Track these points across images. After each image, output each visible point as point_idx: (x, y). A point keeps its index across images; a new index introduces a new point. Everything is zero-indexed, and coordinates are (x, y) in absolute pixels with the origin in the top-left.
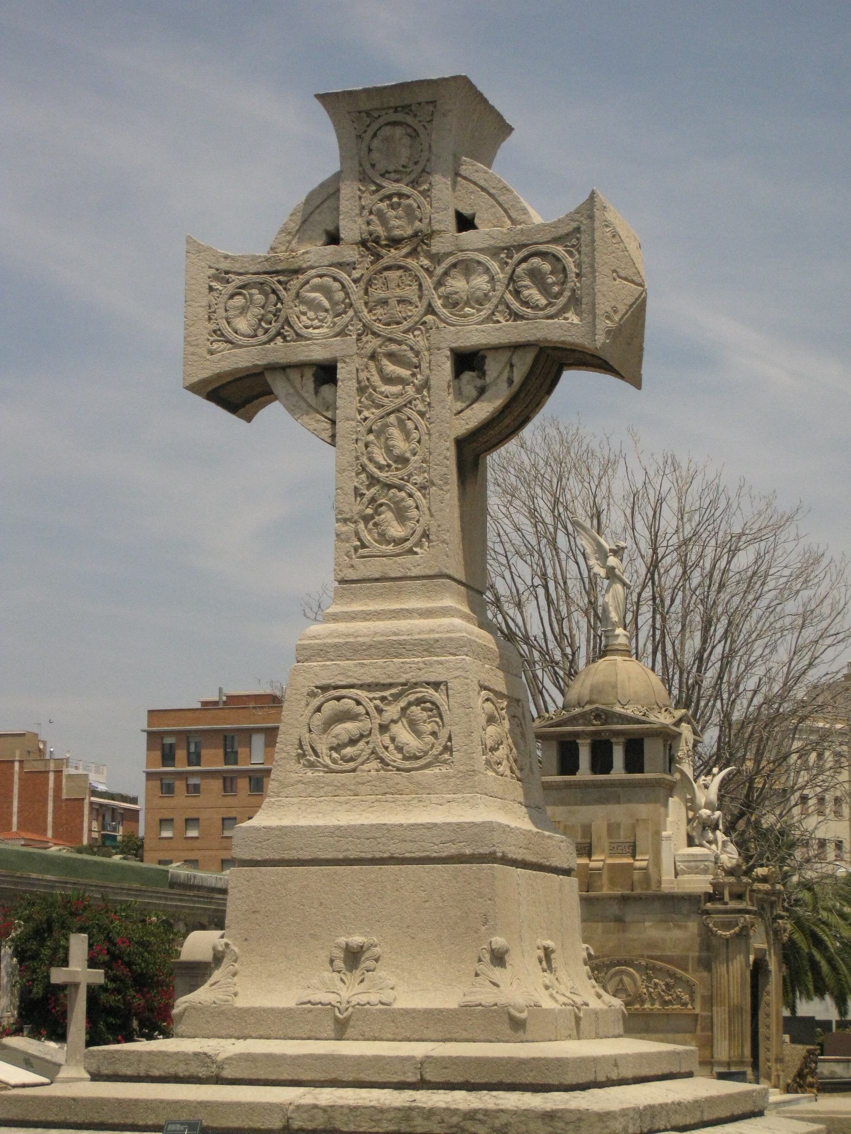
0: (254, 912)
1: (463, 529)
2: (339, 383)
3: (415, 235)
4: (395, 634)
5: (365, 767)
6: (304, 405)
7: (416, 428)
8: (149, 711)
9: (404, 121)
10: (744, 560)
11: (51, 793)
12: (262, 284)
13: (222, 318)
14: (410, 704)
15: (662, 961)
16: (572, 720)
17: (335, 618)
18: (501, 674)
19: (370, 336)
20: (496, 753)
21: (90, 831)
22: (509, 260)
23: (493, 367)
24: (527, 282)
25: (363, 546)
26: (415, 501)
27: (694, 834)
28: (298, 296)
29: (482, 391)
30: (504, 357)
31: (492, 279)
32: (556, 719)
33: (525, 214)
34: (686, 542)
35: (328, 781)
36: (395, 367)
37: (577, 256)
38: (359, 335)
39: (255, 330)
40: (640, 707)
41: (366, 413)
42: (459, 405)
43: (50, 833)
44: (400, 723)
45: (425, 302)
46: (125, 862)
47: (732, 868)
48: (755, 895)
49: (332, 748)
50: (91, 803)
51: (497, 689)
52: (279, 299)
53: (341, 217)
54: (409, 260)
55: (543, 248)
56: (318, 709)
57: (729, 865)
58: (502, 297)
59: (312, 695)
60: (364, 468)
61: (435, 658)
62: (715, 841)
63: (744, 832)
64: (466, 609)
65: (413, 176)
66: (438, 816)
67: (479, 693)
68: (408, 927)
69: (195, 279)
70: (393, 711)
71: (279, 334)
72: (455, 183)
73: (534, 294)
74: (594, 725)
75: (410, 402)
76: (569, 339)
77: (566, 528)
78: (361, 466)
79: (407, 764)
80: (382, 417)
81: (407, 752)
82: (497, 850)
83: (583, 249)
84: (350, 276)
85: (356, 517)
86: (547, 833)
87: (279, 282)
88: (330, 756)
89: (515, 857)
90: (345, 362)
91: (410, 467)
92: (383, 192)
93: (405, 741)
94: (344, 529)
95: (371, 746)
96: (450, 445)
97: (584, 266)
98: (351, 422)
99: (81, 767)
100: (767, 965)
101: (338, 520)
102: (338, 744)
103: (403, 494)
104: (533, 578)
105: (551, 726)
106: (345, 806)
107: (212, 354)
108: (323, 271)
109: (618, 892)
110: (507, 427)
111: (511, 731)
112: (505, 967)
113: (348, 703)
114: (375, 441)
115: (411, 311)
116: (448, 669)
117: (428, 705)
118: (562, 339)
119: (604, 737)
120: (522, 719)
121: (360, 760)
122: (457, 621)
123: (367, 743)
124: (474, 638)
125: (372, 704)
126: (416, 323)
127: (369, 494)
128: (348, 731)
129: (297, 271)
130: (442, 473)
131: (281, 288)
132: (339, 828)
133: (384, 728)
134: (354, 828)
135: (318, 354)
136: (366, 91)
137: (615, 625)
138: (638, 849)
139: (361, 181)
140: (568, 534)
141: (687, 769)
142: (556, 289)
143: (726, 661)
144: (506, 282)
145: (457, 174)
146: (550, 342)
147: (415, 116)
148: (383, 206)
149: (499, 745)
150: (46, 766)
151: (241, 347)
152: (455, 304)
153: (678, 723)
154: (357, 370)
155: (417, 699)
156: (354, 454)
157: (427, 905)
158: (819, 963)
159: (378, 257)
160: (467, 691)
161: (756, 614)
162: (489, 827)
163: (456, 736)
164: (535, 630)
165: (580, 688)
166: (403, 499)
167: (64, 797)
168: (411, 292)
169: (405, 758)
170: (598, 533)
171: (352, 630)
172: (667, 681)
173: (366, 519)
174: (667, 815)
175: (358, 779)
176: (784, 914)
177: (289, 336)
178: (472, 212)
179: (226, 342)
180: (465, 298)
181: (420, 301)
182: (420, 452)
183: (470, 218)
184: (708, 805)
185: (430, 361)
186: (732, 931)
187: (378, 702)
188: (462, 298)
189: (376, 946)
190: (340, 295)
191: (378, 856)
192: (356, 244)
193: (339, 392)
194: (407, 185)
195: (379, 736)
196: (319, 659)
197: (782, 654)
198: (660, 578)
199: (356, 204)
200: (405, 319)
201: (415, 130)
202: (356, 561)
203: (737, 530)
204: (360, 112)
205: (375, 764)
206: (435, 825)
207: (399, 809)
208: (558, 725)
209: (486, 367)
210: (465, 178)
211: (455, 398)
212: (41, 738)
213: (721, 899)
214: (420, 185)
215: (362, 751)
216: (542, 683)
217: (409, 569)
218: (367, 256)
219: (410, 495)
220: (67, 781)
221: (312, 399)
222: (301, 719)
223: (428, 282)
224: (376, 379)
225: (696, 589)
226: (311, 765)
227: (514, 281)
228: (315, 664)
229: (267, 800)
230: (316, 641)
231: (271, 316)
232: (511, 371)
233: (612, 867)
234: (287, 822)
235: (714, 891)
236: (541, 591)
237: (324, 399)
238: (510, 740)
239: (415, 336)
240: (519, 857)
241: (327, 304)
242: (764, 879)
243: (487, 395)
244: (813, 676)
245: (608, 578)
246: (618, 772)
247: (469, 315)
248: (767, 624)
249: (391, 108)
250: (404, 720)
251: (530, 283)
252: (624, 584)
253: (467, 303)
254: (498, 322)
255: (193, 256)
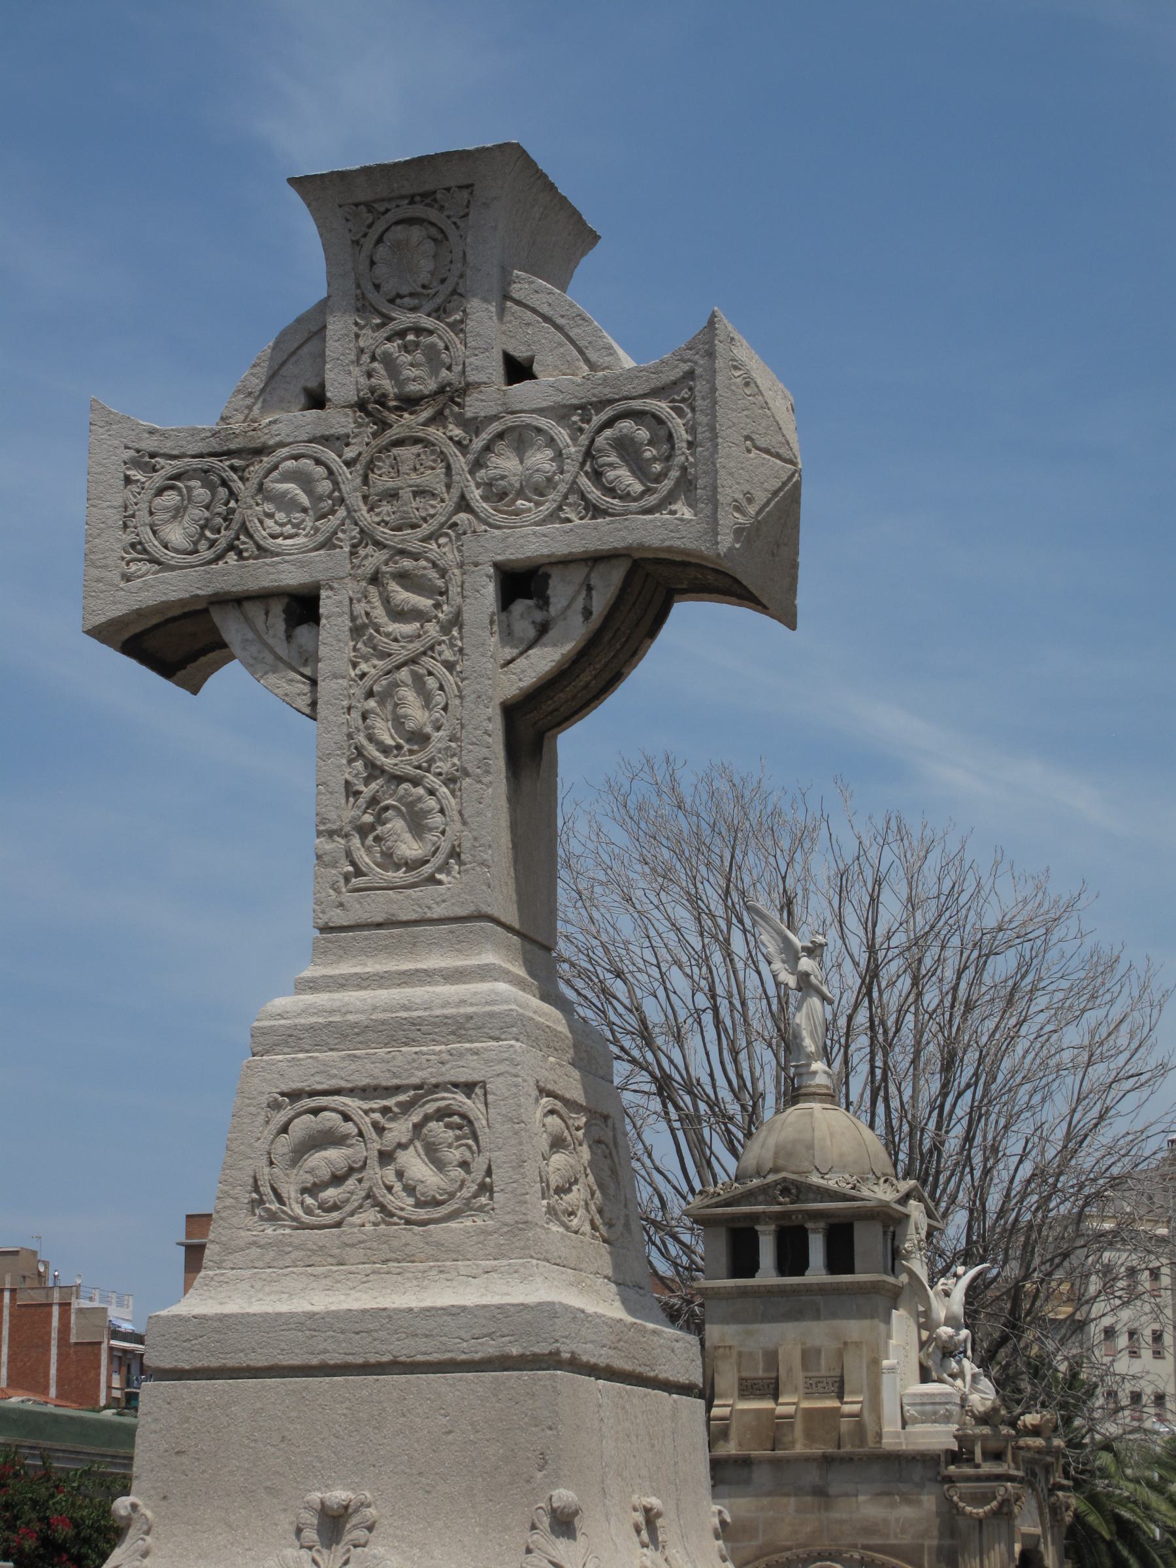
0: (178, 1453)
1: (515, 846)
2: (323, 621)
3: (441, 390)
4: (406, 1008)
5: (356, 1219)
6: (270, 658)
7: (441, 688)
8: (188, 1217)
9: (422, 215)
10: (1001, 967)
11: (54, 1335)
12: (206, 472)
13: (144, 525)
14: (427, 1118)
15: (885, 1553)
16: (748, 1197)
17: (313, 985)
18: (576, 1074)
19: (370, 548)
20: (567, 1198)
21: (109, 1387)
22: (585, 426)
23: (560, 592)
24: (613, 458)
25: (359, 873)
26: (439, 801)
27: (930, 1363)
28: (260, 488)
29: (543, 629)
30: (578, 574)
31: (559, 456)
32: (724, 1195)
33: (611, 354)
34: (917, 942)
35: (297, 1242)
36: (410, 594)
37: (690, 415)
38: (354, 546)
39: (196, 543)
40: (847, 1176)
41: (364, 667)
42: (509, 653)
43: (53, 1391)
44: (411, 1148)
45: (455, 492)
46: (118, 1419)
47: (986, 1413)
48: (1022, 1453)
49: (304, 1191)
50: (111, 1349)
51: (568, 1096)
52: (232, 494)
53: (328, 366)
54: (431, 430)
55: (636, 404)
56: (284, 1129)
57: (982, 1409)
58: (574, 482)
59: (275, 1106)
60: (360, 752)
61: (468, 1045)
62: (961, 1374)
63: (1008, 1365)
64: (521, 972)
65: (439, 300)
66: (469, 1295)
67: (537, 1100)
68: (420, 1474)
69: (103, 466)
70: (400, 1130)
71: (231, 547)
72: (502, 312)
73: (623, 476)
74: (780, 1204)
75: (432, 648)
76: (677, 543)
77: (741, 921)
78: (356, 748)
79: (423, 1214)
80: (388, 673)
81: (422, 1194)
82: (563, 1348)
83: (699, 403)
84: (340, 456)
85: (348, 828)
86: (651, 1326)
87: (233, 468)
88: (302, 1203)
89: (593, 1360)
90: (331, 588)
91: (432, 748)
92: (392, 326)
93: (419, 1176)
94: (328, 846)
95: (366, 1185)
96: (495, 712)
97: (700, 429)
98: (340, 681)
99: (97, 1298)
100: (1041, 1559)
101: (319, 834)
102: (315, 1184)
103: (420, 791)
104: (693, 995)
105: (717, 1205)
106: (324, 1282)
107: (128, 580)
108: (300, 449)
109: (818, 1450)
110: (586, 686)
111: (591, 1163)
112: (575, 1539)
113: (330, 1119)
114: (378, 710)
115: (433, 507)
116: (486, 1061)
117: (456, 1119)
118: (667, 543)
119: (796, 1220)
120: (611, 1145)
121: (348, 1208)
122: (502, 987)
123: (360, 1181)
124: (531, 1014)
125: (367, 1120)
126: (442, 525)
127: (368, 791)
128: (329, 1162)
129: (260, 451)
130: (481, 757)
131: (235, 477)
132: (311, 1316)
133: (386, 1157)
134: (336, 1315)
135: (291, 577)
136: (366, 171)
137: (810, 1057)
138: (847, 1387)
139: (358, 310)
140: (745, 931)
141: (919, 1266)
142: (657, 467)
143: (976, 1116)
144: (581, 459)
145: (507, 297)
146: (649, 549)
147: (442, 208)
148: (392, 347)
149: (571, 1184)
150: (47, 1296)
151: (173, 568)
152: (502, 495)
153: (904, 1200)
154: (351, 600)
155: (438, 1110)
156: (345, 729)
157: (450, 1437)
158: (1127, 1560)
159: (385, 425)
160: (515, 1096)
161: (1021, 1046)
162: (549, 1311)
163: (499, 1167)
164: (700, 1072)
165: (760, 1150)
166: (420, 799)
167: (73, 1340)
168: (434, 478)
169: (419, 1204)
170: (788, 928)
171: (338, 1004)
172: (892, 1148)
173: (363, 831)
174: (889, 1336)
175: (345, 1239)
176: (1065, 1482)
177: (247, 550)
178: (529, 353)
179: (150, 561)
180: (517, 485)
181: (448, 492)
182: (446, 725)
183: (525, 364)
184: (950, 1321)
185: (463, 583)
186: (987, 1508)
187: (377, 1116)
188: (511, 485)
189: (369, 1506)
190: (325, 486)
191: (372, 1360)
192: (351, 406)
193: (323, 634)
194: (429, 315)
195: (377, 1170)
196: (286, 1050)
197: (1060, 1105)
198: (881, 994)
199: (352, 345)
200: (425, 520)
201: (442, 231)
202: (347, 897)
203: (990, 922)
204: (357, 205)
205: (372, 1214)
206: (464, 1308)
207: (408, 1285)
208: (727, 1204)
209: (549, 592)
210: (518, 303)
211: (502, 639)
212: (41, 1256)
213: (970, 1461)
214: (449, 315)
215: (352, 1193)
216: (710, 1148)
217: (429, 908)
218: (367, 425)
219: (432, 792)
220: (77, 1318)
221: (282, 649)
222: (256, 1144)
223: (460, 462)
224: (379, 614)
225: (935, 1011)
226: (272, 1217)
227: (593, 457)
228: (280, 1057)
229: (202, 1274)
230: (282, 1022)
231: (219, 520)
232: (589, 596)
233: (809, 1414)
234: (232, 1307)
235: (960, 1448)
236: (708, 1018)
237: (300, 646)
238: (591, 1178)
239: (439, 546)
240: (602, 1362)
241: (304, 500)
242: (1036, 1431)
243: (552, 634)
244: (1106, 1135)
245: (799, 989)
246: (817, 1273)
247: (523, 511)
248: (1038, 1061)
249: (402, 197)
250: (418, 1144)
251: (618, 460)
252: (824, 998)
253: (520, 494)
254: (569, 520)
255: (101, 430)
